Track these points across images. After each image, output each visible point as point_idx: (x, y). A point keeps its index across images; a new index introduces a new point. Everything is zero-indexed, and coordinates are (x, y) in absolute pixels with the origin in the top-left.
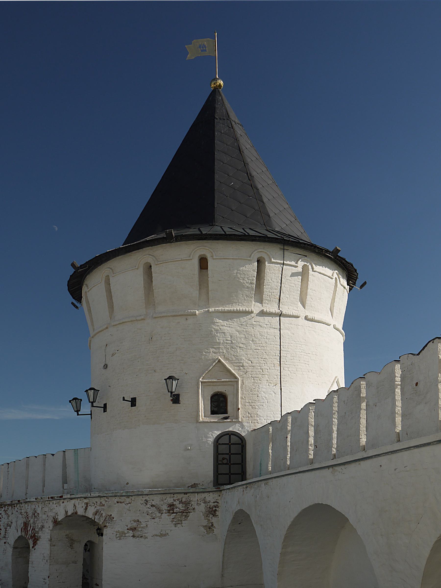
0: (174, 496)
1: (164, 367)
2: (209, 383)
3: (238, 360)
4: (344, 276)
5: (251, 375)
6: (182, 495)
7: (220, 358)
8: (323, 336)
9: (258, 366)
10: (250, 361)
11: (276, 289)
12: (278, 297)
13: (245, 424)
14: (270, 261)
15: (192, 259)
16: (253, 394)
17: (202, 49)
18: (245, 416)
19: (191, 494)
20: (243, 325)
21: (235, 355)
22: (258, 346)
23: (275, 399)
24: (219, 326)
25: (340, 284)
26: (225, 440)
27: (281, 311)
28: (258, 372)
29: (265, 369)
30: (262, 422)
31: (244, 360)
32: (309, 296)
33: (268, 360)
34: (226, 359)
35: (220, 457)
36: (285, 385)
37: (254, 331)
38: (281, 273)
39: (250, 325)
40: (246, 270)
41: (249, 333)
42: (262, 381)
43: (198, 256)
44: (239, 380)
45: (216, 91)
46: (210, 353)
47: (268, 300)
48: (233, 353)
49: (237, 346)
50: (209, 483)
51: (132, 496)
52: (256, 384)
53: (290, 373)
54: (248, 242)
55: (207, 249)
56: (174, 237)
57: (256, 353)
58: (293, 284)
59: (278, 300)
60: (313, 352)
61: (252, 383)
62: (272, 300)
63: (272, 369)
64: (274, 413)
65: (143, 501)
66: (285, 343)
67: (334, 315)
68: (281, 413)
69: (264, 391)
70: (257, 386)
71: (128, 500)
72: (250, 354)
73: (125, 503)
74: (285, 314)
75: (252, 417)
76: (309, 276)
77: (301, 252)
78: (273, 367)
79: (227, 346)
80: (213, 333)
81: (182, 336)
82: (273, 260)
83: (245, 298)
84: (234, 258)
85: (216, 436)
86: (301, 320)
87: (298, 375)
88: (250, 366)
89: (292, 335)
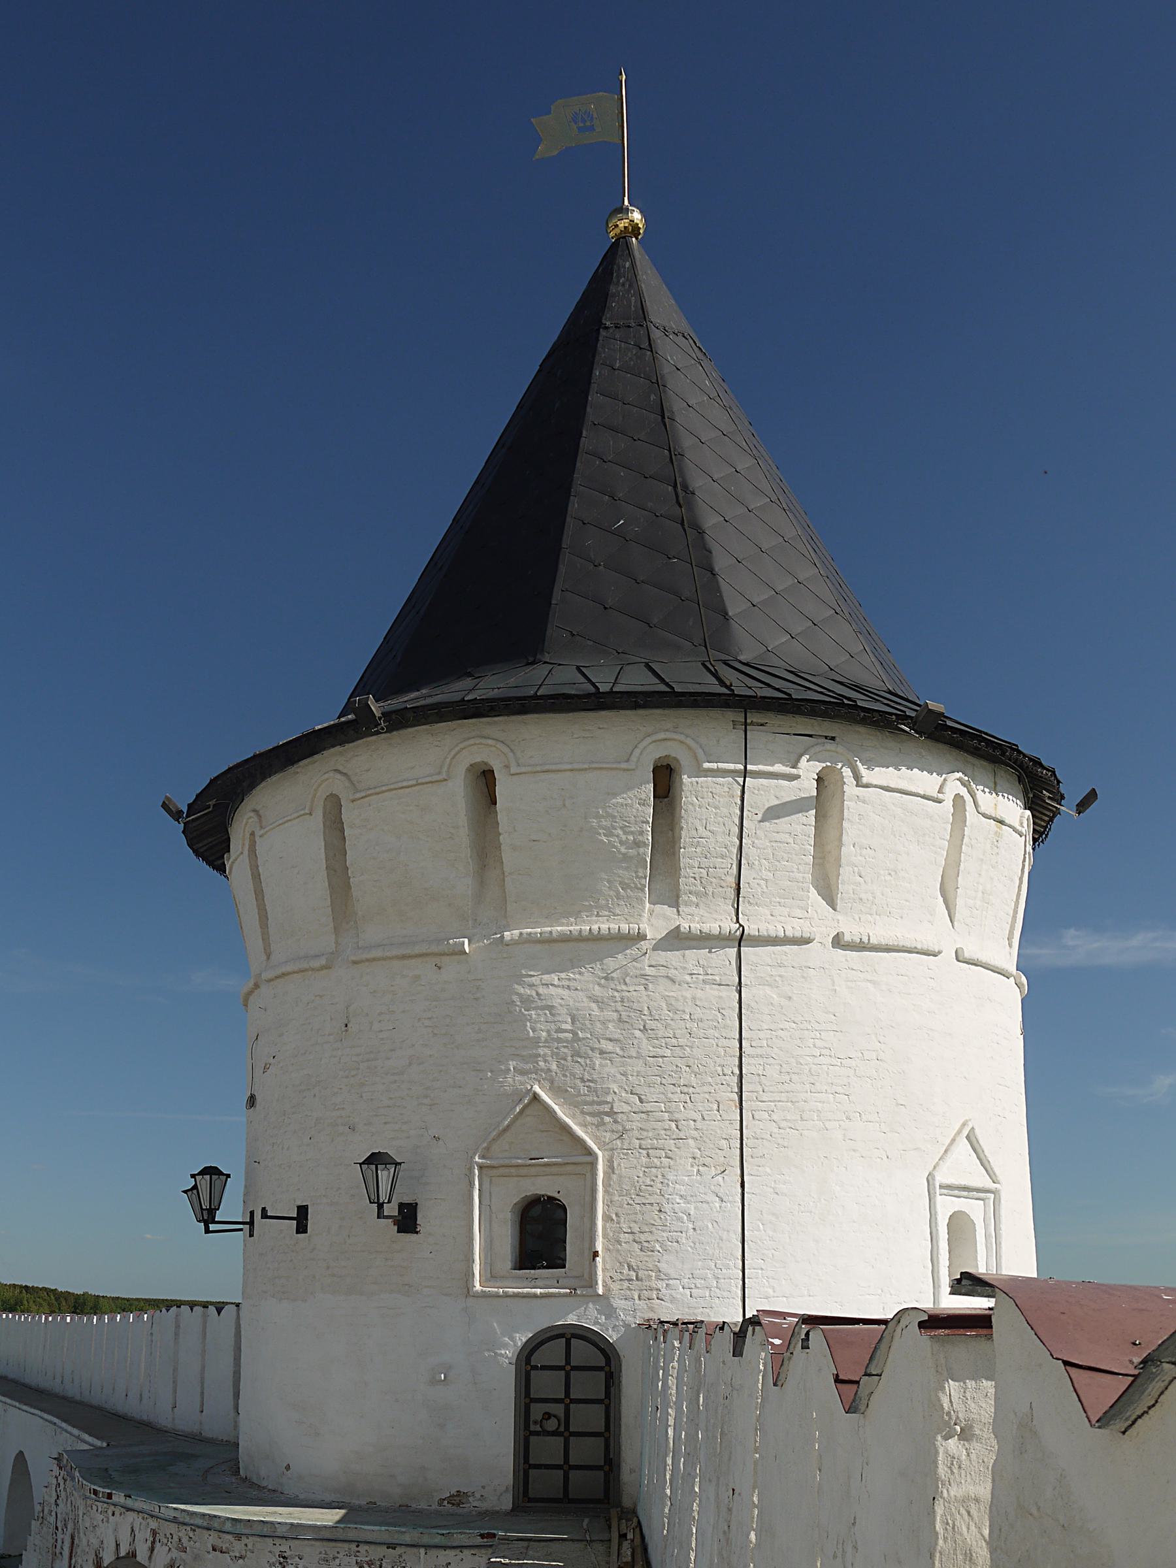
0: (357, 1549)
1: (376, 1115)
2: (507, 1170)
3: (594, 1093)
4: (998, 781)
5: (638, 1141)
6: (383, 1550)
7: (537, 1089)
8: (909, 994)
9: (664, 1110)
10: (635, 1096)
11: (722, 857)
12: (732, 880)
13: (619, 1301)
14: (699, 768)
15: (446, 778)
16: (644, 1204)
17: (581, 125)
18: (617, 1276)
19: (408, 1550)
20: (612, 979)
21: (587, 1077)
22: (663, 1045)
23: (720, 1219)
24: (534, 988)
25: (979, 813)
26: (553, 1353)
27: (741, 925)
28: (663, 1132)
29: (687, 1120)
30: (674, 1295)
31: (615, 1093)
32: (847, 868)
33: (697, 1090)
34: (557, 1091)
35: (537, 1410)
36: (758, 1170)
37: (648, 996)
38: (739, 802)
39: (635, 979)
40: (618, 803)
41: (632, 1004)
42: (676, 1161)
43: (464, 770)
44: (597, 1159)
45: (619, 247)
46: (508, 1074)
47: (697, 894)
48: (578, 1071)
49: (592, 1049)
50: (501, 1494)
51: (247, 1535)
52: (654, 1170)
53: (776, 1130)
54: (622, 712)
55: (491, 746)
56: (380, 718)
57: (655, 1070)
58: (787, 836)
59: (733, 892)
60: (866, 1053)
61: (642, 1166)
62: (710, 893)
63: (710, 1120)
64: (717, 1266)
65: (275, 1556)
66: (759, 1030)
67: (957, 917)
68: (741, 1263)
69: (682, 1193)
70: (657, 1177)
71: (238, 1547)
72: (635, 1074)
73: (231, 1554)
74: (754, 936)
75: (641, 1280)
76: (843, 803)
77: (813, 726)
78: (715, 1112)
79: (562, 1049)
80: (517, 1008)
81: (425, 1019)
82: (706, 765)
83: (618, 891)
84: (576, 766)
85: (524, 1340)
86: (820, 953)
87: (805, 1132)
88: (634, 1113)
89: (784, 1002)
